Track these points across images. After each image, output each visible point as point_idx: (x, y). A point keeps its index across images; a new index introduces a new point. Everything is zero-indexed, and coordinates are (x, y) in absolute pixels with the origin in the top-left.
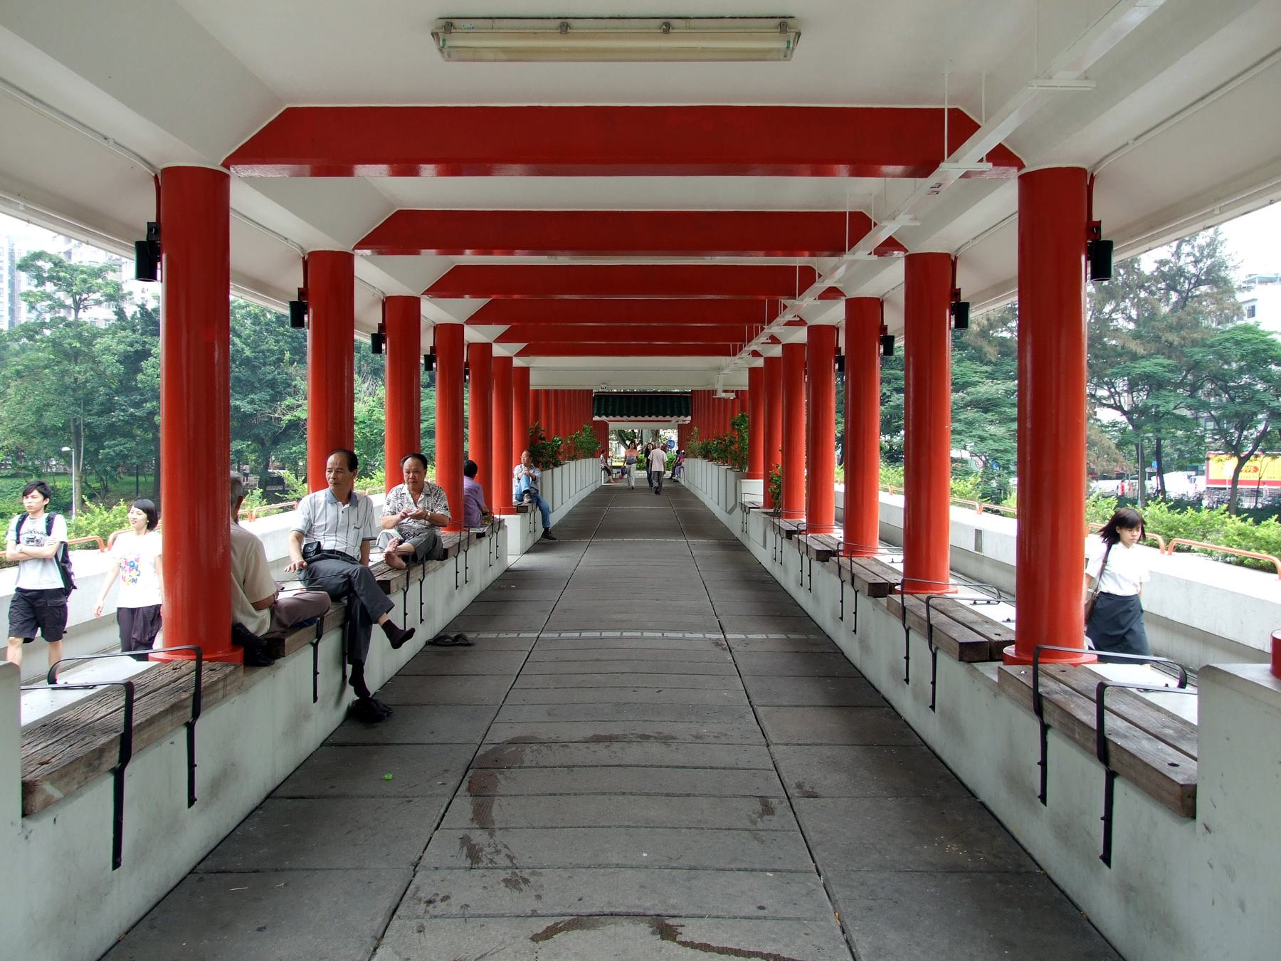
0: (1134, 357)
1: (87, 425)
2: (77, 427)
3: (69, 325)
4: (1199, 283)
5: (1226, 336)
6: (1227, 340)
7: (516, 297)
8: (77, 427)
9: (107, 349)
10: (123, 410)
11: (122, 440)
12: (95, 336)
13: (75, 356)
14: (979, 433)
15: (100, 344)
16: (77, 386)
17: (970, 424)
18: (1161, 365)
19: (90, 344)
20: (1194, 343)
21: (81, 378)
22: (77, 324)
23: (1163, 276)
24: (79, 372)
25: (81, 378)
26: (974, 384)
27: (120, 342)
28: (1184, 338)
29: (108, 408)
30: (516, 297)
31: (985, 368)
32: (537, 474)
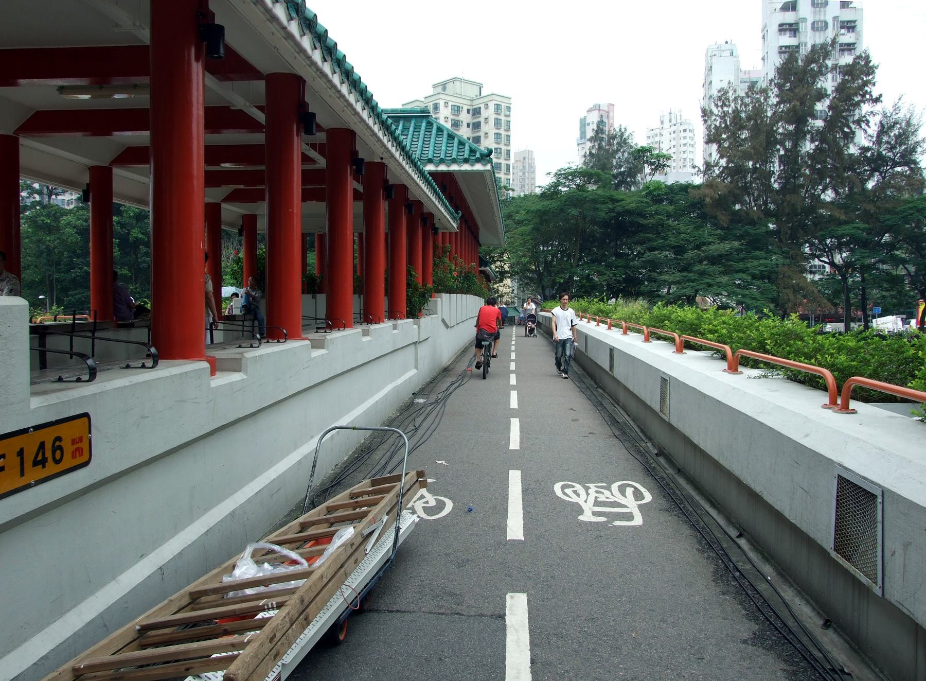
0: (840, 223)
1: (57, 280)
2: (51, 282)
3: (44, 207)
4: (896, 164)
5: (910, 205)
6: (910, 208)
7: (226, 166)
8: (51, 282)
9: (69, 224)
10: (80, 269)
11: (80, 290)
12: (62, 215)
13: (49, 229)
14: (707, 281)
15: (64, 220)
16: (49, 251)
17: (702, 274)
18: (858, 228)
19: (57, 220)
20: (888, 211)
21: (52, 245)
22: (49, 206)
23: (869, 161)
24: (49, 241)
25: (52, 245)
26: (710, 243)
27: (78, 219)
28: (879, 208)
29: (71, 266)
30: (226, 166)
31: (719, 231)
32: (901, 356)
